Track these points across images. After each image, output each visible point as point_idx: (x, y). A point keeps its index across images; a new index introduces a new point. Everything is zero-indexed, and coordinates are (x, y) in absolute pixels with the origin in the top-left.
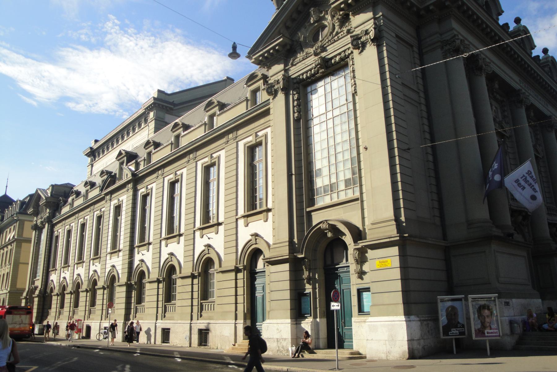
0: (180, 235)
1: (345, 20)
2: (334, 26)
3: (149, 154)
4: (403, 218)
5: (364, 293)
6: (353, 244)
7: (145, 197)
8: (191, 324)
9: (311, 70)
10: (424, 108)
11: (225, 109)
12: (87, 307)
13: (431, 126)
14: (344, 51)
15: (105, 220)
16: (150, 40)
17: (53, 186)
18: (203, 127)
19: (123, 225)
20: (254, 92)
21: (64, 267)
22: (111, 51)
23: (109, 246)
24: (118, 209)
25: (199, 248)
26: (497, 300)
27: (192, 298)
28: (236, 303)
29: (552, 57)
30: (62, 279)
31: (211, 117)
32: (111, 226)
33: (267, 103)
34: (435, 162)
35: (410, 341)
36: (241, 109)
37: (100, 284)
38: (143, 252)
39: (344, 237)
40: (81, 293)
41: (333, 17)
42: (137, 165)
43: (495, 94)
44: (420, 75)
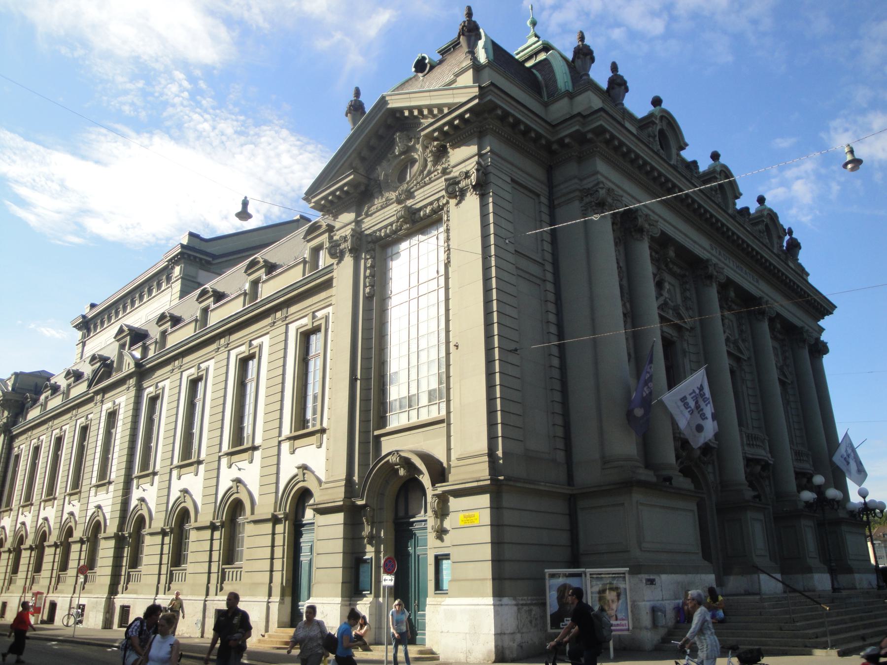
0: (199, 462)
1: (441, 153)
2: (426, 161)
3: (164, 334)
4: (500, 453)
5: (444, 562)
6: (431, 488)
7: (154, 400)
8: (269, 602)
9: (391, 224)
10: (550, 287)
11: (274, 273)
12: (55, 572)
13: (559, 313)
14: (438, 200)
15: (92, 433)
16: (237, 121)
17: (17, 375)
18: (242, 298)
19: (118, 442)
20: (316, 251)
21: (23, 507)
22: (172, 137)
23: (95, 474)
24: (112, 416)
25: (288, 470)
26: (627, 576)
27: (210, 562)
28: (272, 571)
29: (771, 210)
30: (19, 525)
31: (255, 284)
32: (99, 443)
33: (329, 269)
34: (563, 368)
35: (499, 635)
36: (295, 275)
37: (78, 534)
38: (144, 486)
39: (421, 476)
40: (47, 549)
41: (425, 148)
42: (145, 349)
43: (671, 266)
44: (547, 238)
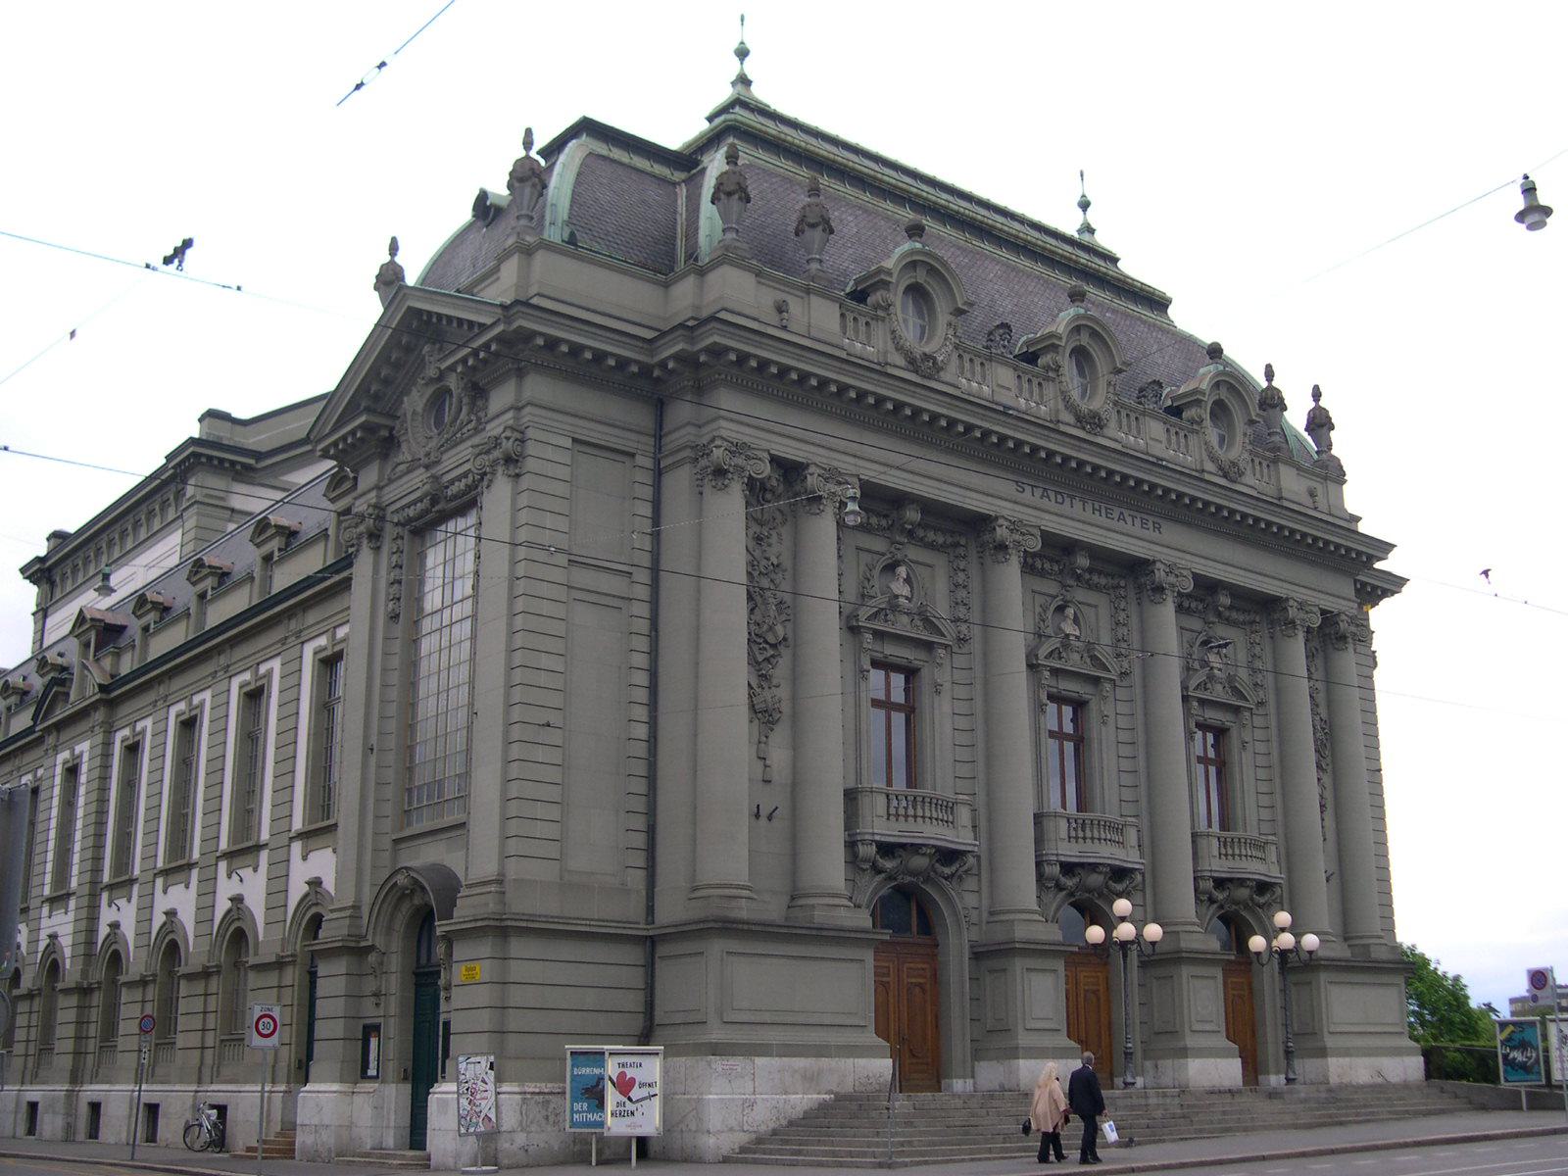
24: (72, 771)
43: (921, 533)
